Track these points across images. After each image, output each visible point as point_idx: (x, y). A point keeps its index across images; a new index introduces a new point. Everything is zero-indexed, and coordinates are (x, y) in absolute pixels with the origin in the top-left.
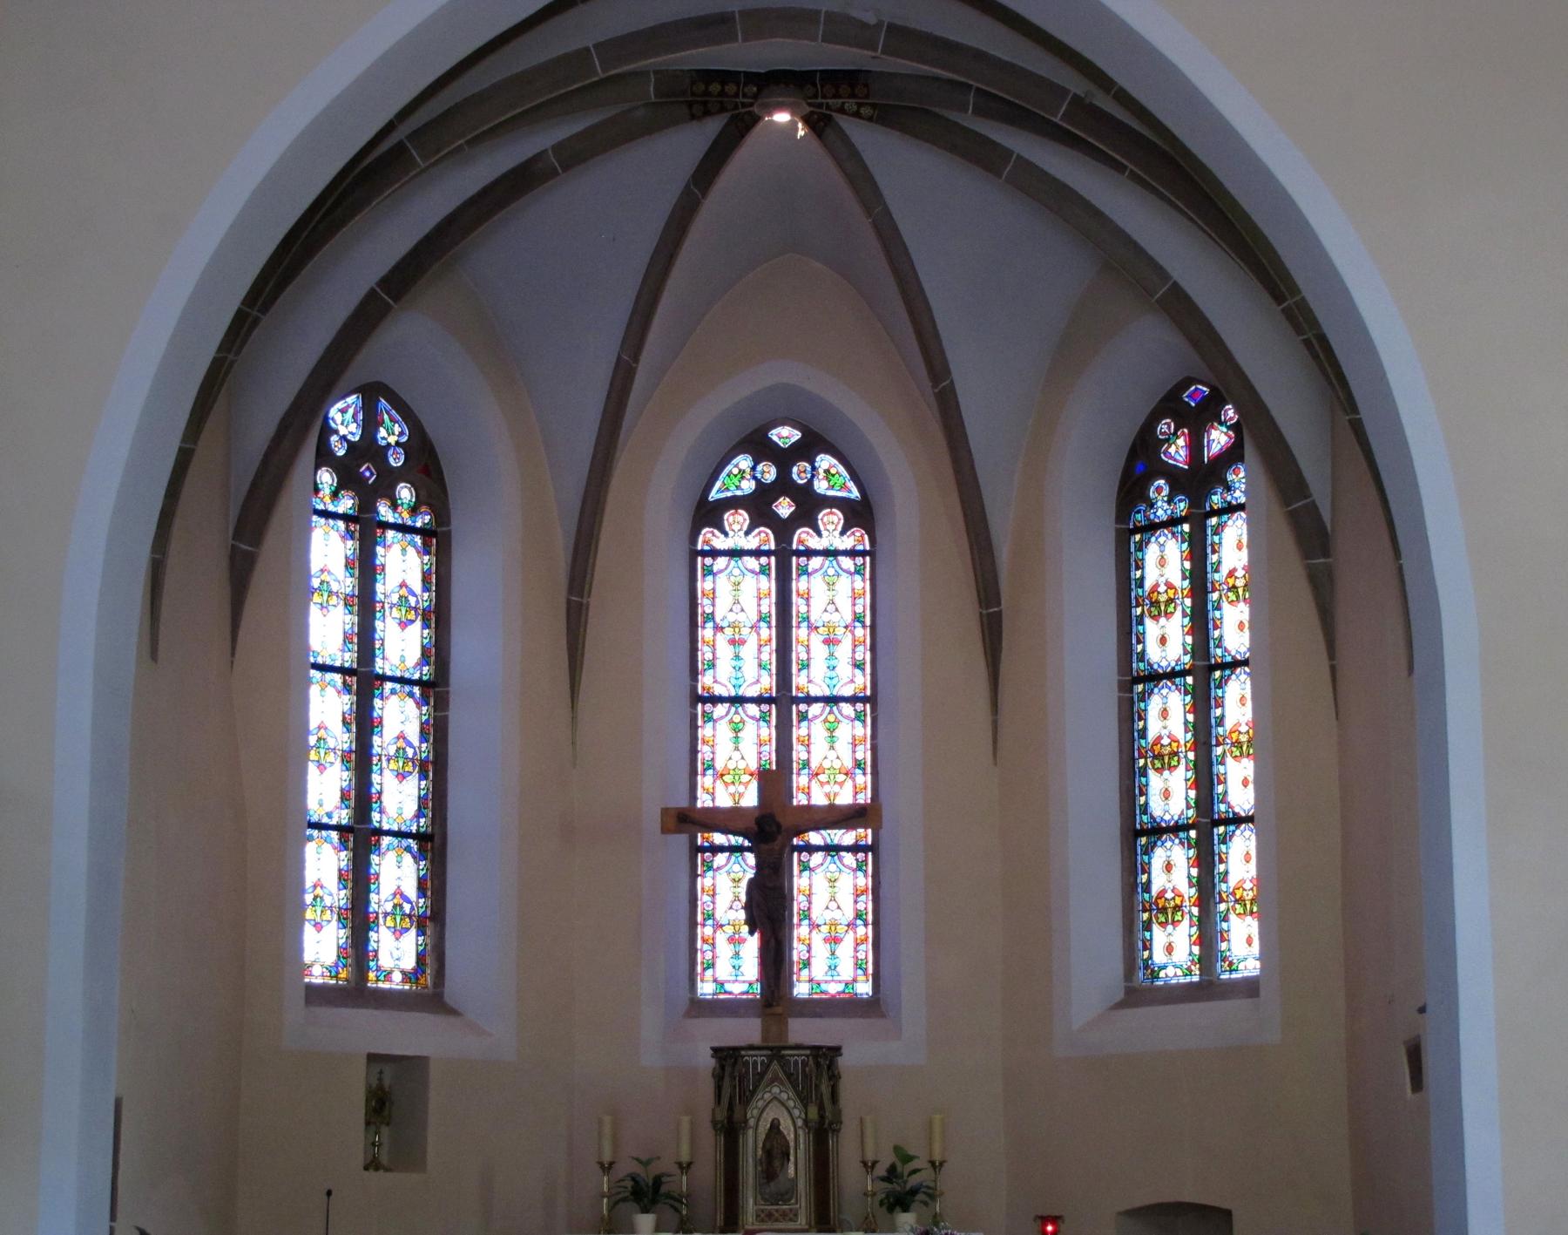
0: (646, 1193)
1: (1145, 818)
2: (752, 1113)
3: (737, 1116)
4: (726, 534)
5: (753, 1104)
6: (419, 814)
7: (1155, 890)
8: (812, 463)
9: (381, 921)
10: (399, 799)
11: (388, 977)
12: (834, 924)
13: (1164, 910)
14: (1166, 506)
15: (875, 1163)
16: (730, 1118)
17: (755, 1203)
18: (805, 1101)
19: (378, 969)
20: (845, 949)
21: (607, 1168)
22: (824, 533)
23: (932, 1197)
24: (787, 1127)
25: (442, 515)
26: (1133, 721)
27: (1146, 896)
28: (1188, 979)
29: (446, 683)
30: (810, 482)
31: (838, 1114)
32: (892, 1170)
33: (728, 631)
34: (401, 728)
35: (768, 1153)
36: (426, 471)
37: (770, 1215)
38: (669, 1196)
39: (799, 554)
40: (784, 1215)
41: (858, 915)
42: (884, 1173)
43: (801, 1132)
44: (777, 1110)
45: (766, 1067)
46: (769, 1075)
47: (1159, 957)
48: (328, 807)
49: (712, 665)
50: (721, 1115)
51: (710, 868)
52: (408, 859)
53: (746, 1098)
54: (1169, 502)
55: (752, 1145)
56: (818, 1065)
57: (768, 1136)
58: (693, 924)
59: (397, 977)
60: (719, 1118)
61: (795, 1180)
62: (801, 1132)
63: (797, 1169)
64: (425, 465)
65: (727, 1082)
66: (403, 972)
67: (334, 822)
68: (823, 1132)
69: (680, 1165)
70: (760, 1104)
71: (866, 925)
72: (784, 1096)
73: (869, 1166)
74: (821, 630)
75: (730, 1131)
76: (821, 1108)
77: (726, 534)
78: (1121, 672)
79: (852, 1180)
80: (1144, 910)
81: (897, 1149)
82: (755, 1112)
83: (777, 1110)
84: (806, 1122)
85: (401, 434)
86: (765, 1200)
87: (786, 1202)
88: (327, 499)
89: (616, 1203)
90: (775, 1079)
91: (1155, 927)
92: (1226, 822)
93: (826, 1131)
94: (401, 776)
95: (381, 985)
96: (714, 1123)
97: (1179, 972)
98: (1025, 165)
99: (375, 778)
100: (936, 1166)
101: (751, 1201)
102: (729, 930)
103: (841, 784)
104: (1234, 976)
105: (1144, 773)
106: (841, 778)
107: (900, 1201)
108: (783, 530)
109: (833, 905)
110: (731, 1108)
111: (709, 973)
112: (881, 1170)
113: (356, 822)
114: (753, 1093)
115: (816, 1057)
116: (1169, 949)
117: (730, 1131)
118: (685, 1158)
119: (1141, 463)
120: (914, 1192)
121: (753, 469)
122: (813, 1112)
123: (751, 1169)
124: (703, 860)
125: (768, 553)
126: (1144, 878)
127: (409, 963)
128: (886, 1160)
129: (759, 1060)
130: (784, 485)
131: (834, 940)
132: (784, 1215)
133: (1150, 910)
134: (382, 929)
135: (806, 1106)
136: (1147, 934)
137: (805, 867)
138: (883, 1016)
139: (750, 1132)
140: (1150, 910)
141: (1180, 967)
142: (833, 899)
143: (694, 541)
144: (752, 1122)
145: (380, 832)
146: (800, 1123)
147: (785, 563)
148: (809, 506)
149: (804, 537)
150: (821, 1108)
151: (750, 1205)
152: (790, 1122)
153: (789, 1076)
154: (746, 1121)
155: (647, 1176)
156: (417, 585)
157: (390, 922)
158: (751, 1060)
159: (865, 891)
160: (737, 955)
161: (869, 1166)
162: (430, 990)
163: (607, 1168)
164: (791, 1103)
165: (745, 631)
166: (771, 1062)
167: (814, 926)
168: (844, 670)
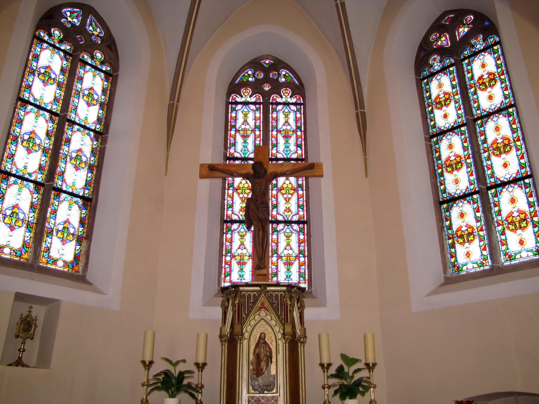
0: (171, 383)
1: (445, 195)
2: (247, 329)
4: (242, 97)
6: (85, 188)
7: (455, 228)
8: (278, 71)
9: (55, 233)
10: (75, 178)
11: (55, 262)
12: (288, 256)
13: (462, 236)
14: (439, 64)
15: (329, 365)
17: (248, 392)
19: (49, 257)
20: (295, 268)
21: (148, 365)
22: (284, 97)
23: (367, 389)
24: (270, 339)
25: (115, 68)
26: (433, 154)
27: (450, 232)
28: (482, 268)
29: (107, 133)
30: (278, 79)
32: (340, 369)
33: (242, 132)
34: (81, 147)
35: (258, 356)
36: (109, 47)
38: (189, 385)
39: (272, 104)
41: (300, 252)
43: (280, 343)
44: (263, 326)
45: (256, 298)
46: (259, 304)
47: (461, 259)
48: (30, 170)
49: (234, 144)
51: (230, 230)
52: (75, 208)
53: (240, 319)
54: (440, 62)
55: (246, 351)
57: (257, 345)
58: (221, 255)
59: (60, 263)
61: (275, 377)
62: (280, 343)
63: (278, 369)
64: (110, 45)
66: (64, 262)
67: (33, 178)
68: (294, 344)
69: (197, 364)
70: (253, 323)
71: (304, 257)
73: (325, 367)
74: (282, 132)
75: (232, 342)
77: (242, 97)
78: (425, 133)
79: (313, 379)
80: (449, 238)
81: (344, 357)
82: (249, 329)
83: (263, 326)
84: (284, 334)
85: (100, 33)
86: (253, 389)
88: (56, 41)
89: (152, 390)
90: (263, 306)
91: (457, 246)
92: (495, 186)
94: (77, 168)
95: (49, 266)
96: (221, 336)
97: (475, 266)
99: (62, 165)
100: (370, 367)
102: (238, 258)
103: (292, 194)
104: (513, 262)
105: (442, 175)
106: (292, 192)
107: (349, 390)
108: (266, 95)
109: (288, 247)
110: (232, 327)
111: (228, 278)
112: (332, 370)
113: (46, 182)
114: (247, 315)
115: (289, 291)
116: (468, 255)
117: (232, 342)
118: (201, 361)
119: (424, 53)
120: (358, 383)
121: (254, 74)
122: (288, 329)
124: (227, 227)
125: (260, 104)
126: (448, 223)
127: (70, 257)
128: (337, 362)
129: (252, 294)
130: (267, 80)
131: (289, 264)
133: (453, 238)
134: (55, 238)
135: (284, 325)
136: (453, 250)
137: (275, 231)
138: (314, 297)
139: (245, 342)
140: (453, 238)
141: (476, 263)
142: (288, 244)
143: (228, 98)
144: (246, 335)
145: (60, 191)
146: (279, 336)
147: (266, 107)
148: (277, 88)
149: (275, 98)
153: (272, 304)
154: (243, 335)
155: (175, 371)
156: (99, 92)
157: (60, 235)
159: (304, 241)
160: (241, 270)
161: (325, 367)
162: (77, 274)
163: (148, 365)
165: (249, 132)
166: (260, 295)
167: (279, 257)
168: (293, 148)
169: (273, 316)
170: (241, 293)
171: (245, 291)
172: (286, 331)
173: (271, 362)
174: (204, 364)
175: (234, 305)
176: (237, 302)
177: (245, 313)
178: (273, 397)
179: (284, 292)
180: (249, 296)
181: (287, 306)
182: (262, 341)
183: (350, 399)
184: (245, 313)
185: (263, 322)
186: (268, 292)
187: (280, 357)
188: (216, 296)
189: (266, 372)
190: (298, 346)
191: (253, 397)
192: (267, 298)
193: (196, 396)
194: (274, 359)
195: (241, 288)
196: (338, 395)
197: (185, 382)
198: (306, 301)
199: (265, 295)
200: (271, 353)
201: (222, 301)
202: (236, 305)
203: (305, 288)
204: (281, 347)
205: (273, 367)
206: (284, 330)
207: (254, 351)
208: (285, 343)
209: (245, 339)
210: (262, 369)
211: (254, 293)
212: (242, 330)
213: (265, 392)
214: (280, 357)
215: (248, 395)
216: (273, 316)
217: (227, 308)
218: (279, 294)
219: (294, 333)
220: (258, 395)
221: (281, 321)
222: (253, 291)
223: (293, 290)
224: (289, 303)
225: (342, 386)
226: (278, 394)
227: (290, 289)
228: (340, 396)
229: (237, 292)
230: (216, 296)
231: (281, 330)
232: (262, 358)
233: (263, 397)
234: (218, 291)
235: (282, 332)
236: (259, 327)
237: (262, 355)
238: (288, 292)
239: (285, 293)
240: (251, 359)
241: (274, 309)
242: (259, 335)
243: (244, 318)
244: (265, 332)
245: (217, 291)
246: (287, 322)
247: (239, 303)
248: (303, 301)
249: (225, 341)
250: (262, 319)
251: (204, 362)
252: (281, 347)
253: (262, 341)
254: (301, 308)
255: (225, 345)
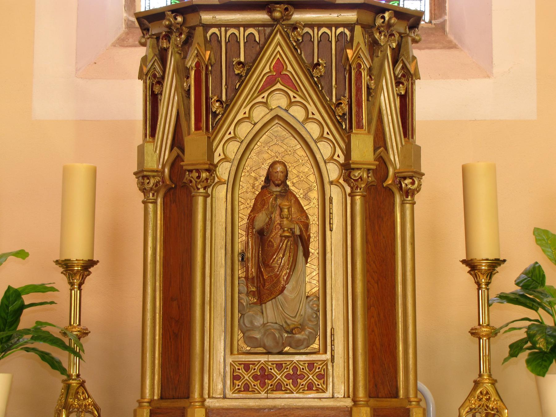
3: (194, 151)
5: (227, 128)
15: (495, 264)
16: (176, 164)
18: (345, 123)
24: (302, 180)
31: (413, 154)
32: (533, 280)
35: (261, 236)
37: (263, 376)
38: (39, 333)
40: (295, 376)
42: (512, 288)
43: (335, 193)
45: (257, 50)
46: (265, 67)
50: (158, 157)
53: (207, 113)
55: (223, 218)
56: (374, 45)
57: (260, 203)
60: (152, 163)
62: (335, 193)
63: (328, 276)
65: (170, 83)
68: (382, 193)
69: (66, 266)
70: (244, 130)
72: (298, 112)
76: (380, 141)
79: (441, 306)
81: (542, 237)
82: (233, 149)
84: (347, 168)
86: (249, 340)
87: (299, 346)
93: (389, 192)
96: (142, 175)
98: (357, 95)
101: (220, 346)
110: (177, 142)
112: (507, 281)
114: (227, 106)
117: (176, 191)
118: (77, 253)
122: (363, 148)
123: (221, 272)
129: (242, 34)
132: (295, 376)
138: (451, 46)
139: (221, 193)
144: (224, 171)
146: (333, 172)
150: (380, 141)
151: (217, 355)
152: (308, 168)
153: (310, 69)
154: (212, 169)
158: (224, 35)
164: (313, 129)
166: (268, 39)
169: (311, 108)
170: (206, 31)
171: (219, 26)
172: (355, 156)
173: (307, 254)
174: (89, 264)
175: (183, 72)
176: (191, 63)
177: (219, 100)
178: (311, 365)
179: (351, 27)
180: (234, 40)
181: (359, 74)
182: (275, 182)
183: (508, 302)
184: (219, 100)
185: (277, 129)
186: (294, 27)
187: (335, 238)
188: (121, 42)
189: (289, 287)
190: (393, 205)
191: (247, 367)
192: (294, 50)
193: (65, 365)
194: (314, 248)
195: (206, 17)
196: (524, 355)
197: (27, 320)
198: (423, 57)
199: (286, 37)
200: (307, 226)
201: (144, 60)
202: (188, 70)
203: (422, 13)
204: (337, 209)
205: (312, 270)
206: (348, 154)
207: (252, 219)
208: (352, 195)
209: (221, 183)
210: (278, 276)
211: (340, 30)
212: (211, 153)
213: (287, 349)
214: (335, 238)
215: (230, 360)
216: (311, 108)
217: (160, 82)
218: (333, 34)
219: (382, 163)
220: (263, 359)
221: (338, 124)
222: (246, 26)
223: (379, 21)
224: (366, 64)
225: (536, 329)
226: (328, 356)
227: (367, 17)
228: (528, 362)
229: (193, 28)
230: (121, 42)
231: (338, 151)
232: (274, 242)
233: (279, 366)
234: (129, 25)
235: (342, 160)
236: (267, 143)
237: (275, 237)
238: (364, 27)
239: (352, 31)
240: (239, 247)
241: (315, 85)
242: (266, 167)
243: (215, 114)
244: (287, 159)
245: (123, 28)
246: (360, 126)
247: (198, 65)
248: (414, 58)
249: (156, 190)
250: (277, 117)
251: (86, 258)
252: (337, 209)
253: (275, 182)
254: (406, 77)
255: (155, 203)
